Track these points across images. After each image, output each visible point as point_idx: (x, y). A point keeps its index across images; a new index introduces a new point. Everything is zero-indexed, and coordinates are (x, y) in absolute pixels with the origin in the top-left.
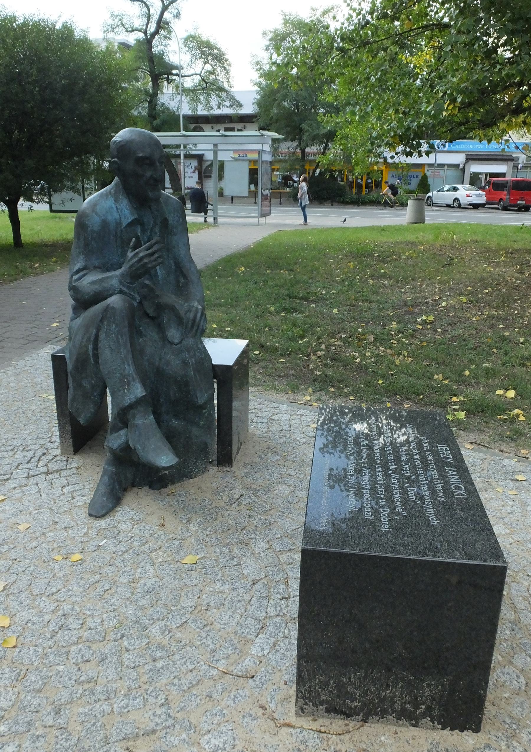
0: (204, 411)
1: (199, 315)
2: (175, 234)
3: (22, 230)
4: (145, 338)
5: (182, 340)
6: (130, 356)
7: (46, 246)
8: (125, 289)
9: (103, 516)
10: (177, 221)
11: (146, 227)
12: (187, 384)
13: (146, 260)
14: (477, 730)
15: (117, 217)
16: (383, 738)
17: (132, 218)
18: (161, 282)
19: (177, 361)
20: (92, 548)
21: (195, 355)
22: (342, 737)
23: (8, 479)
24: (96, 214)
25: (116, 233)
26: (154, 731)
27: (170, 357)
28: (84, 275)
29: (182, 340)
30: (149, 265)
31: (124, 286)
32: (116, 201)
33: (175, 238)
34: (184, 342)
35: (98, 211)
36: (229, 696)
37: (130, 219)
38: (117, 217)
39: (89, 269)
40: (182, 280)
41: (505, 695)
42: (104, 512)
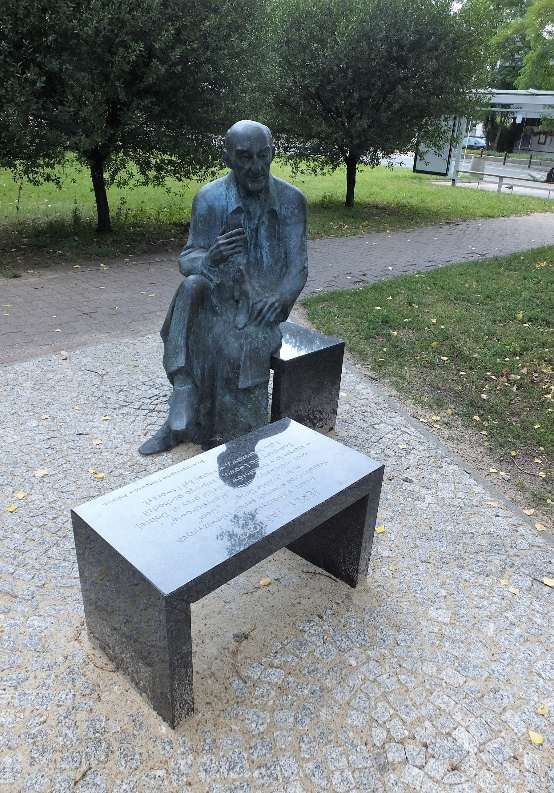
0: (252, 396)
1: (267, 307)
2: (288, 225)
3: (356, 190)
4: (219, 318)
5: (245, 326)
6: (185, 330)
7: (377, 207)
8: (205, 271)
9: (148, 455)
10: (292, 213)
11: (252, 216)
12: (238, 367)
13: (222, 248)
14: (173, 727)
15: (225, 203)
16: (116, 687)
17: (237, 206)
18: (265, 269)
19: (236, 345)
20: (117, 474)
21: (251, 342)
22: (96, 669)
23: (126, 406)
24: (205, 200)
25: (222, 218)
26: (16, 597)
27: (231, 340)
28: (190, 252)
29: (245, 326)
30: (224, 253)
31: (206, 268)
32: (227, 188)
33: (288, 228)
34: (246, 329)
35: (207, 197)
36: (74, 605)
37: (235, 206)
38: (225, 203)
39: (194, 248)
40: (284, 270)
41: (233, 727)
42: (149, 452)
